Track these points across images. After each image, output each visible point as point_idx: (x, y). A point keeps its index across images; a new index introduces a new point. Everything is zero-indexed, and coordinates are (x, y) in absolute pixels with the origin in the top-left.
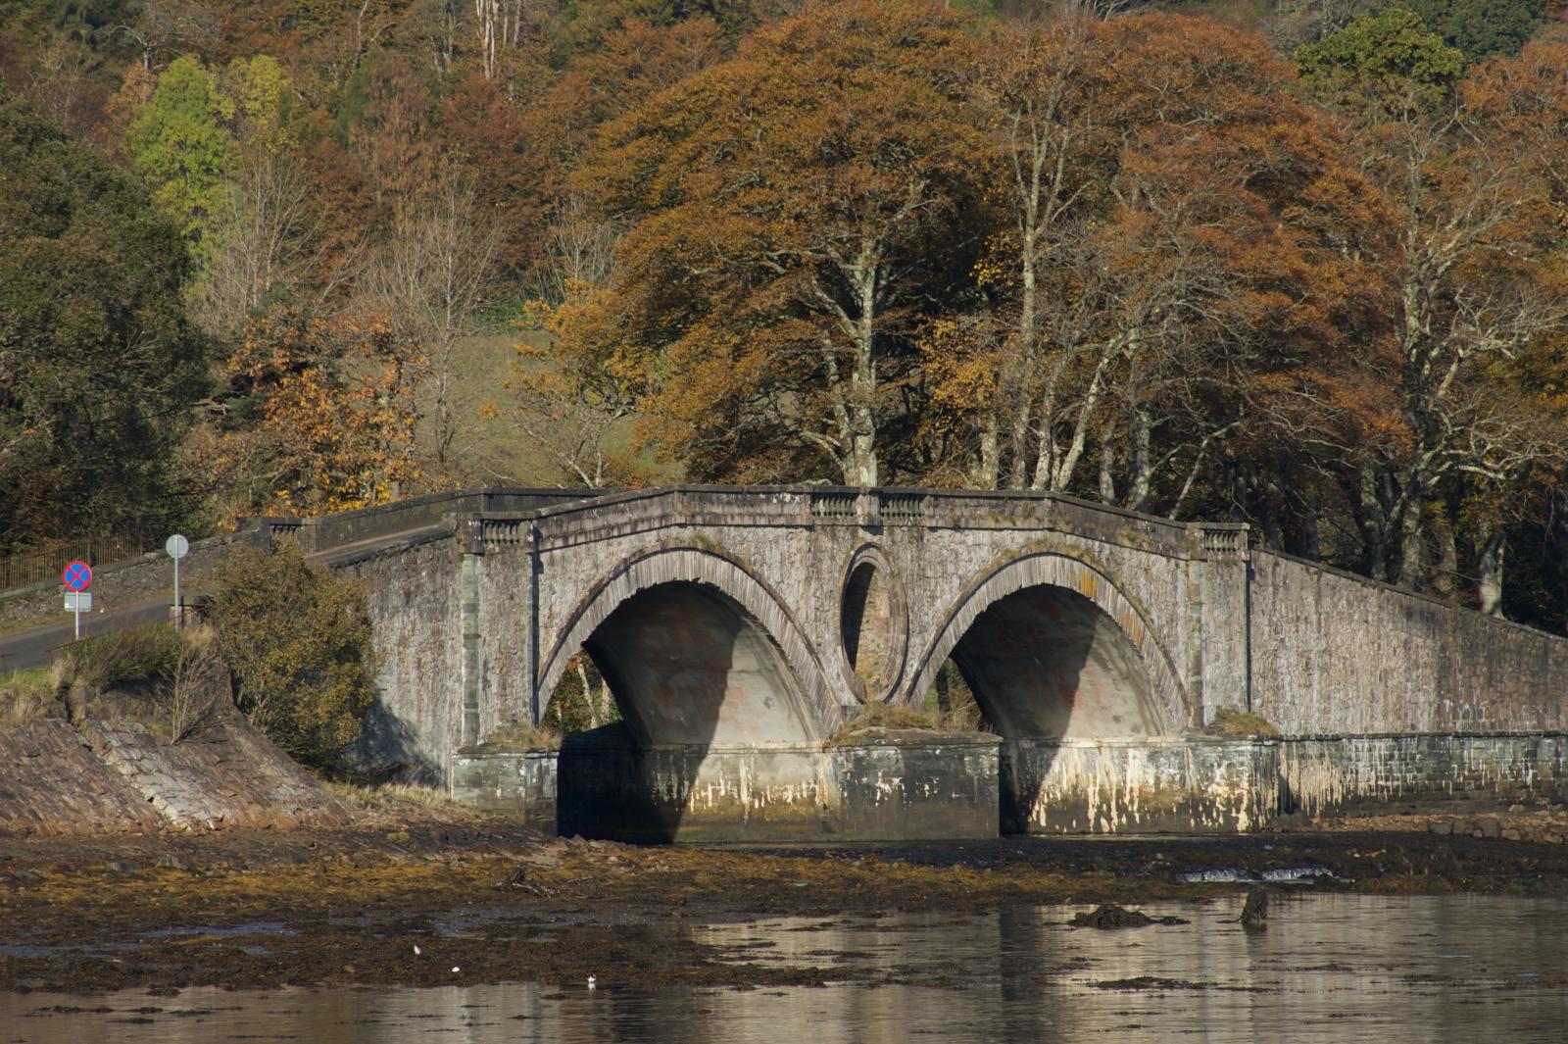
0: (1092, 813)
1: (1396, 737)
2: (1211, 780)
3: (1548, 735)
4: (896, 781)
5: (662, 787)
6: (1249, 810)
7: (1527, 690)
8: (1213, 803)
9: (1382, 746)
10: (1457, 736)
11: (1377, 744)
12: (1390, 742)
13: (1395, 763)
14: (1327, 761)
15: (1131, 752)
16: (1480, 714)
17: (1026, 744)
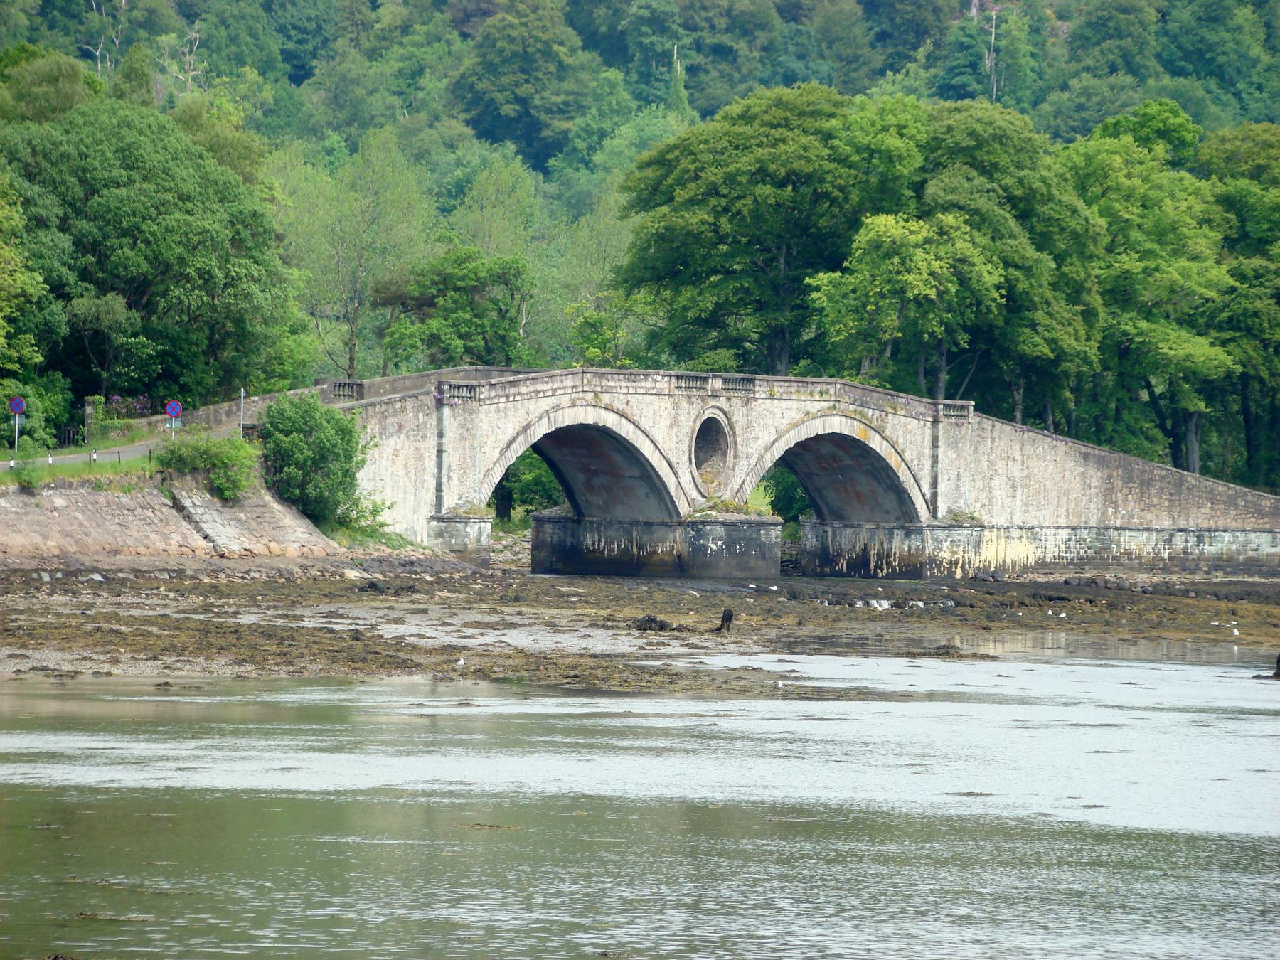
0: (872, 566)
1: (1074, 528)
2: (941, 549)
3: (1180, 530)
4: (720, 543)
5: (590, 542)
6: (963, 567)
7: (1166, 503)
8: (941, 562)
9: (1064, 534)
10: (1116, 529)
11: (1060, 531)
12: (1069, 531)
13: (1072, 543)
14: (1024, 540)
15: (896, 532)
16: (1133, 517)
17: (836, 524)
